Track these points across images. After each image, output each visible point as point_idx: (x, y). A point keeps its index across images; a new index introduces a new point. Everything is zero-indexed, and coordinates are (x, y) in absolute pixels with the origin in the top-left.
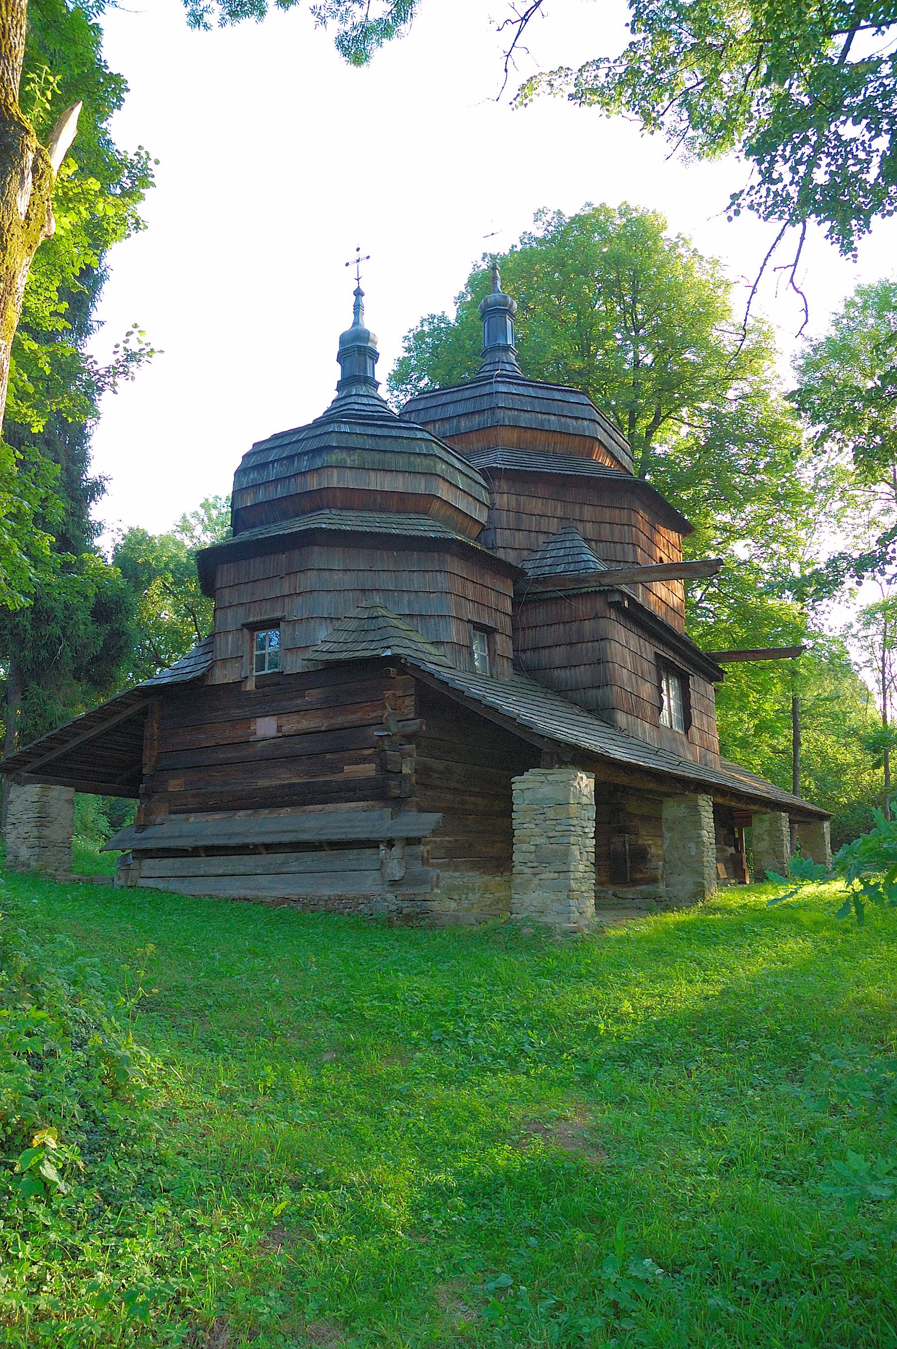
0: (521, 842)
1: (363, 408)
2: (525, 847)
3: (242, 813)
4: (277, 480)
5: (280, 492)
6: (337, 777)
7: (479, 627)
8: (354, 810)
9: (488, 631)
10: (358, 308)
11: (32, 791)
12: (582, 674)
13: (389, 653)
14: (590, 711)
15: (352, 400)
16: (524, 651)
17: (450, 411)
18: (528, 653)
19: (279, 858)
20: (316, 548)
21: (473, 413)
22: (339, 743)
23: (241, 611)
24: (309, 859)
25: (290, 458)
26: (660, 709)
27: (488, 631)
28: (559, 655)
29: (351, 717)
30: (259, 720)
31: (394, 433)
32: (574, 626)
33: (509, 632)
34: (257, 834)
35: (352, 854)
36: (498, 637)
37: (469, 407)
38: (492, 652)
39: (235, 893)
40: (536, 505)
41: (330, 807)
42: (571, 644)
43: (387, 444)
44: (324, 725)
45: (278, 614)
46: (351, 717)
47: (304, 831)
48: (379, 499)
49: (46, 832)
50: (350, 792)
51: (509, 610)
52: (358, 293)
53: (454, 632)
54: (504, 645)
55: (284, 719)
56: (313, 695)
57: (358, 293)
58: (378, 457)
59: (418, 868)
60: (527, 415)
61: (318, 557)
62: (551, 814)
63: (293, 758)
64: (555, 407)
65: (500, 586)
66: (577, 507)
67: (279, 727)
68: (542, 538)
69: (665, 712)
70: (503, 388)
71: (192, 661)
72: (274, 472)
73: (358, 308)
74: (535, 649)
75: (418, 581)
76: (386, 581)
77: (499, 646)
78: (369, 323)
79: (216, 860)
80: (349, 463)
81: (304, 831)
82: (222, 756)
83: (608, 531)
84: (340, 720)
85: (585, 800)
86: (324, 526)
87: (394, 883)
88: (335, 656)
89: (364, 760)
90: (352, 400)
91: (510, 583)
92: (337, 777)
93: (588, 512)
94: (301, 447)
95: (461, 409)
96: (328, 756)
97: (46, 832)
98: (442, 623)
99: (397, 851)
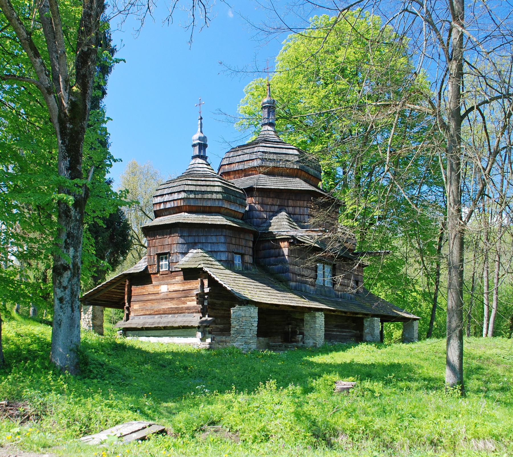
0: (233, 327)
2: (234, 329)
3: (170, 316)
6: (183, 306)
15: (196, 165)
20: (179, 229)
25: (171, 193)
30: (162, 286)
40: (269, 201)
44: (181, 288)
48: (202, 208)
55: (169, 286)
62: (241, 320)
63: (172, 299)
65: (247, 237)
75: (214, 239)
82: (151, 297)
83: (298, 210)
89: (193, 300)
91: (252, 235)
92: (183, 306)
93: (291, 203)
96: (183, 299)
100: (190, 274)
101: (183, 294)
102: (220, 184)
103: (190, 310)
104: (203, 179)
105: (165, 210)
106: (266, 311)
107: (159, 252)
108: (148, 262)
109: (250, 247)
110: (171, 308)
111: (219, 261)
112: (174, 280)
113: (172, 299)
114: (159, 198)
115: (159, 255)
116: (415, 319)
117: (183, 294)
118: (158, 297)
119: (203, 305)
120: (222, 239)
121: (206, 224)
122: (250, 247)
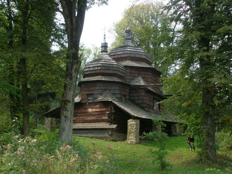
1: (105, 57)
3: (86, 123)
4: (92, 70)
5: (92, 72)
7: (123, 95)
8: (104, 124)
9: (125, 96)
10: (105, 38)
11: (50, 119)
12: (140, 101)
13: (110, 100)
14: (141, 108)
15: (104, 55)
16: (131, 97)
17: (119, 53)
18: (132, 97)
19: (92, 131)
21: (123, 54)
22: (102, 113)
23: (86, 92)
24: (96, 131)
26: (154, 107)
27: (125, 96)
28: (136, 98)
29: (104, 109)
30: (89, 109)
31: (111, 63)
32: (139, 93)
33: (128, 95)
34: (89, 127)
35: (103, 130)
36: (127, 96)
37: (123, 53)
38: (126, 99)
39: (85, 136)
40: (134, 72)
41: (100, 123)
42: (139, 96)
43: (109, 65)
45: (92, 93)
46: (104, 109)
47: (96, 127)
49: (52, 125)
50: (103, 121)
51: (128, 91)
52: (105, 35)
53: (119, 96)
54: (127, 97)
55: (93, 109)
56: (97, 106)
57: (105, 35)
58: (108, 67)
59: (113, 133)
60: (133, 55)
61: (98, 84)
63: (94, 115)
64: (138, 53)
66: (141, 72)
67: (92, 111)
68: (134, 77)
69: (155, 106)
70: (129, 49)
71: (77, 99)
72: (91, 69)
73: (105, 38)
74: (133, 97)
75: (114, 88)
76: (109, 88)
77: (127, 97)
78: (107, 42)
79: (81, 131)
80: (104, 69)
81: (96, 127)
84: (102, 110)
85: (138, 124)
86: (100, 79)
87: (110, 135)
88: (102, 100)
89: (106, 116)
90: (104, 55)
93: (143, 73)
94: (96, 65)
95: (121, 53)
97: (52, 125)
98: (118, 95)
99: (110, 130)
100: (106, 104)
101: (100, 113)
102: (116, 64)
103: (104, 120)
104: (108, 61)
105: (91, 74)
106: (142, 121)
107: (88, 93)
108: (82, 98)
109: (128, 92)
110: (94, 119)
111: (117, 98)
112: (95, 106)
113: (94, 115)
114: (88, 69)
115: (88, 94)
116: (15, 129)
117: (100, 113)
118: (87, 114)
119: (111, 118)
120: (118, 88)
121: (95, 81)
122: (128, 92)
